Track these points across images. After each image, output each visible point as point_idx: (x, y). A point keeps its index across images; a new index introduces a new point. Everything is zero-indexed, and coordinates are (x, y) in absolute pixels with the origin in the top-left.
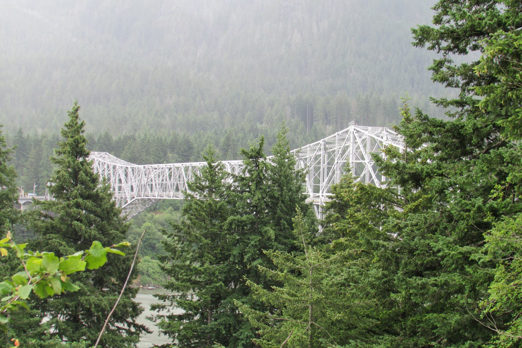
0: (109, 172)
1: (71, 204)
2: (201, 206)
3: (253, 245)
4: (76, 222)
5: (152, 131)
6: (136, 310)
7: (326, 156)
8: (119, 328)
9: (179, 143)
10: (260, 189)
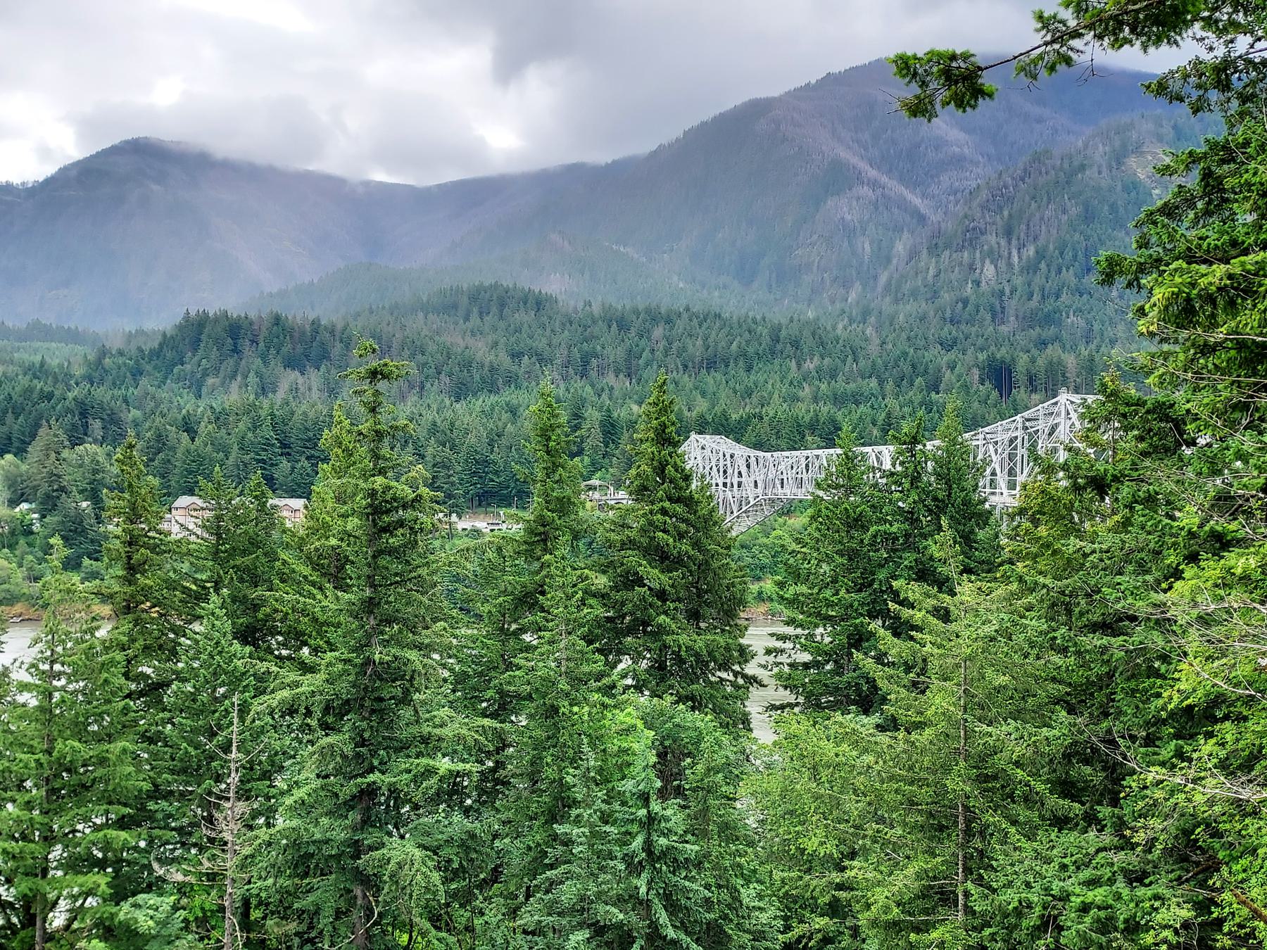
3: (906, 566)
4: (661, 534)
7: (1026, 437)
8: (722, 679)
10: (917, 487)
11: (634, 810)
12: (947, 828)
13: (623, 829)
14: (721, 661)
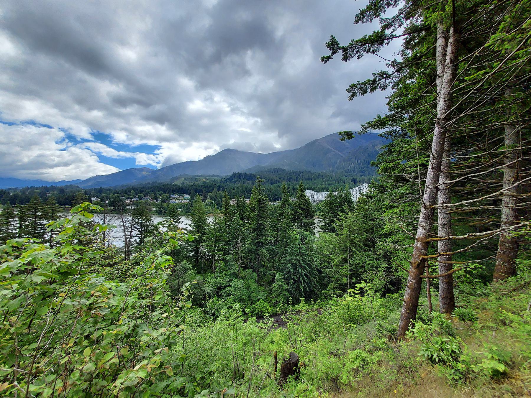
6: (314, 223)
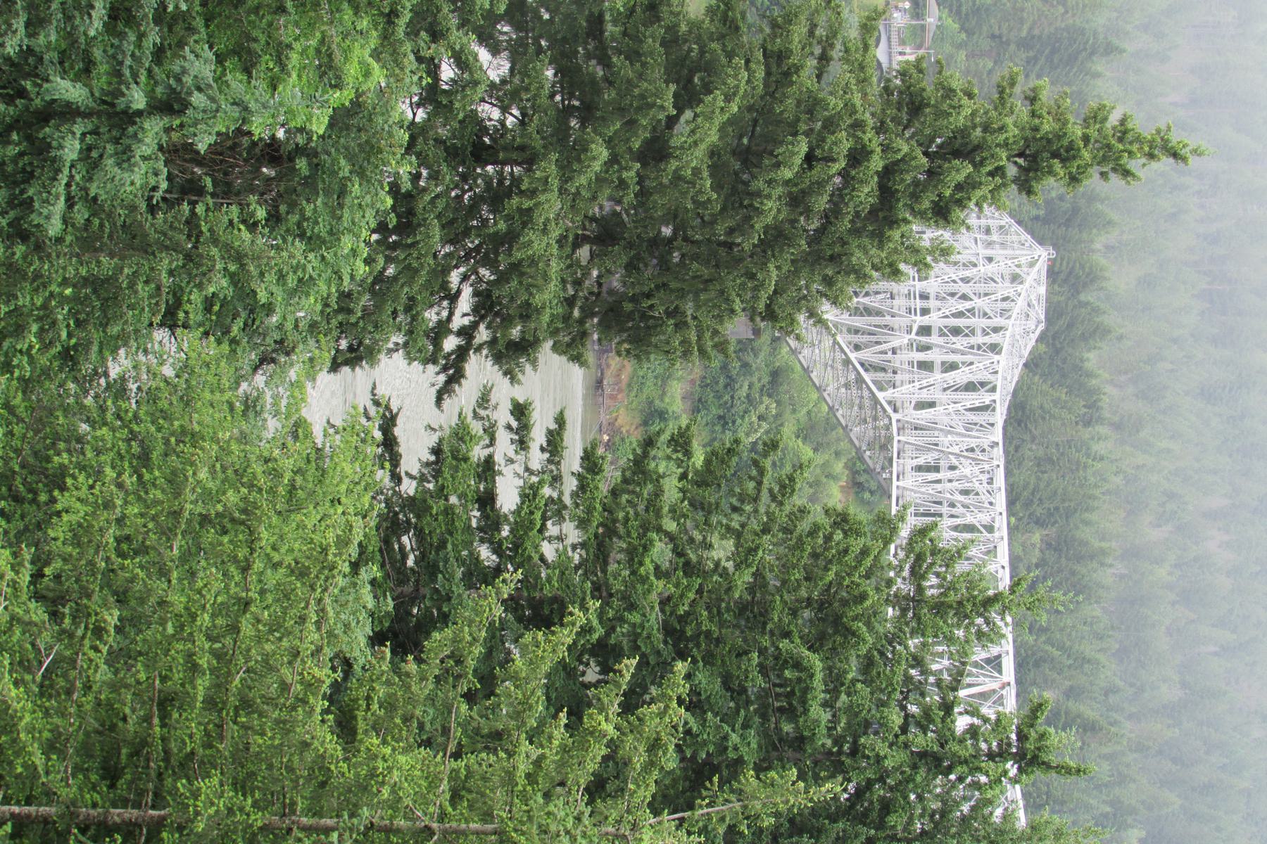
0: (979, 332)
1: (864, 132)
2: (856, 567)
3: (725, 738)
4: (804, 148)
5: (1118, 480)
8: (454, 298)
9: (1077, 567)
10: (915, 767)
11: (143, 78)
12: (112, 786)
13: (97, 53)
14: (496, 293)
